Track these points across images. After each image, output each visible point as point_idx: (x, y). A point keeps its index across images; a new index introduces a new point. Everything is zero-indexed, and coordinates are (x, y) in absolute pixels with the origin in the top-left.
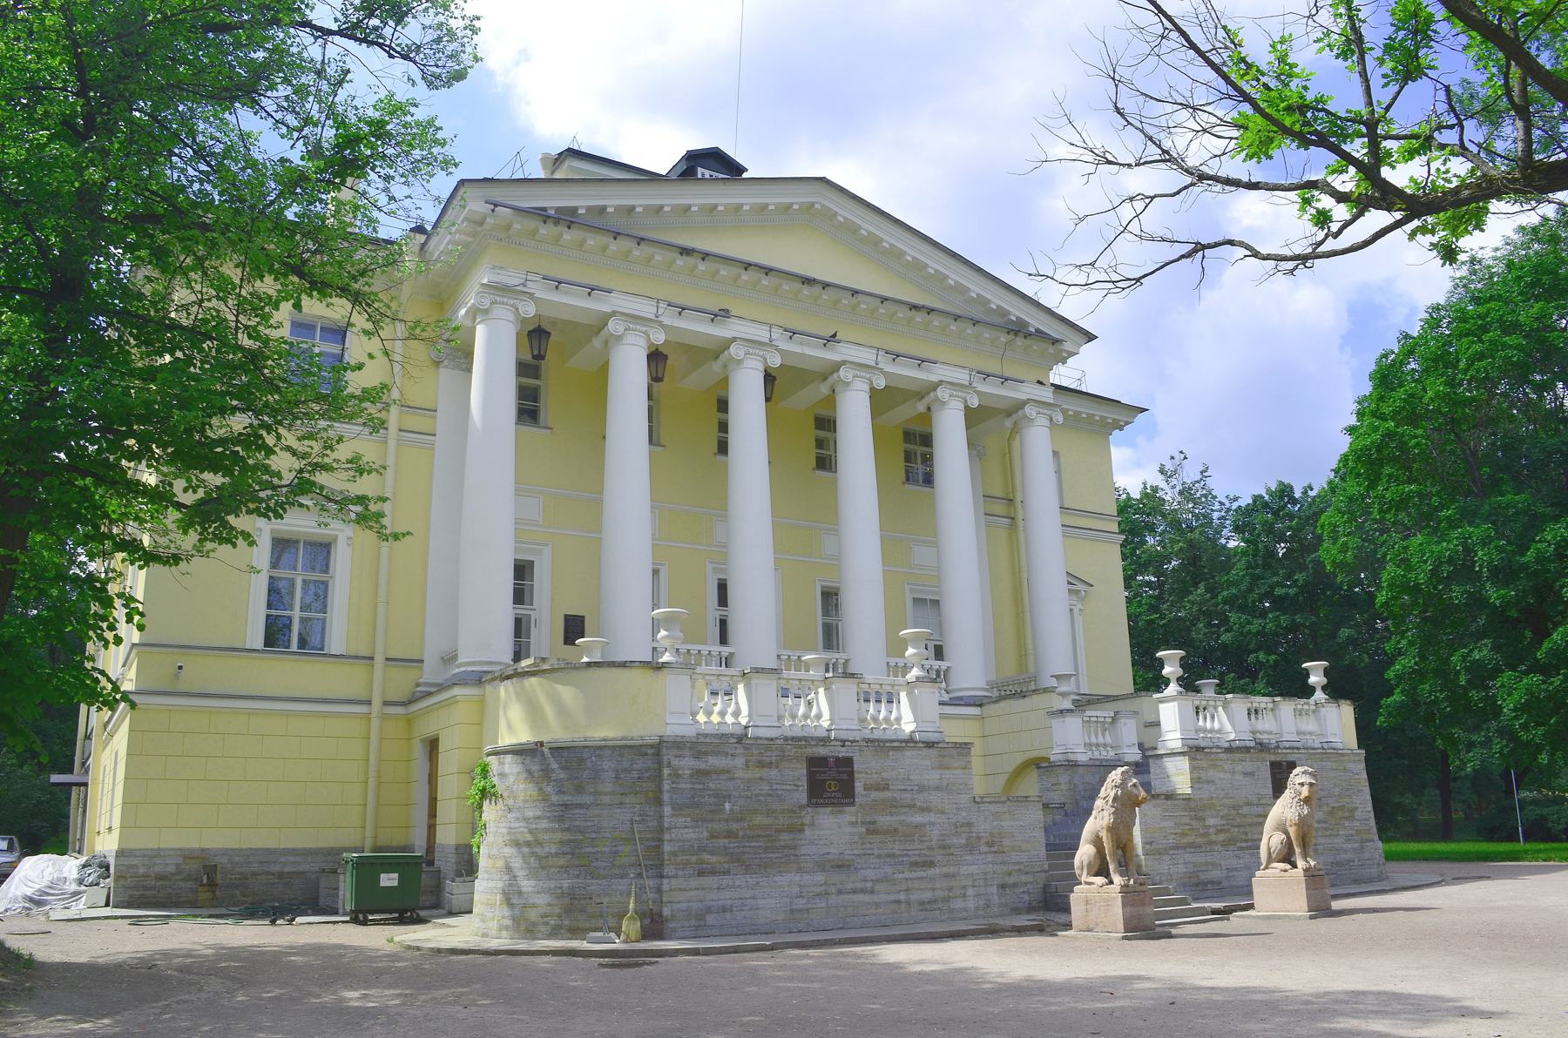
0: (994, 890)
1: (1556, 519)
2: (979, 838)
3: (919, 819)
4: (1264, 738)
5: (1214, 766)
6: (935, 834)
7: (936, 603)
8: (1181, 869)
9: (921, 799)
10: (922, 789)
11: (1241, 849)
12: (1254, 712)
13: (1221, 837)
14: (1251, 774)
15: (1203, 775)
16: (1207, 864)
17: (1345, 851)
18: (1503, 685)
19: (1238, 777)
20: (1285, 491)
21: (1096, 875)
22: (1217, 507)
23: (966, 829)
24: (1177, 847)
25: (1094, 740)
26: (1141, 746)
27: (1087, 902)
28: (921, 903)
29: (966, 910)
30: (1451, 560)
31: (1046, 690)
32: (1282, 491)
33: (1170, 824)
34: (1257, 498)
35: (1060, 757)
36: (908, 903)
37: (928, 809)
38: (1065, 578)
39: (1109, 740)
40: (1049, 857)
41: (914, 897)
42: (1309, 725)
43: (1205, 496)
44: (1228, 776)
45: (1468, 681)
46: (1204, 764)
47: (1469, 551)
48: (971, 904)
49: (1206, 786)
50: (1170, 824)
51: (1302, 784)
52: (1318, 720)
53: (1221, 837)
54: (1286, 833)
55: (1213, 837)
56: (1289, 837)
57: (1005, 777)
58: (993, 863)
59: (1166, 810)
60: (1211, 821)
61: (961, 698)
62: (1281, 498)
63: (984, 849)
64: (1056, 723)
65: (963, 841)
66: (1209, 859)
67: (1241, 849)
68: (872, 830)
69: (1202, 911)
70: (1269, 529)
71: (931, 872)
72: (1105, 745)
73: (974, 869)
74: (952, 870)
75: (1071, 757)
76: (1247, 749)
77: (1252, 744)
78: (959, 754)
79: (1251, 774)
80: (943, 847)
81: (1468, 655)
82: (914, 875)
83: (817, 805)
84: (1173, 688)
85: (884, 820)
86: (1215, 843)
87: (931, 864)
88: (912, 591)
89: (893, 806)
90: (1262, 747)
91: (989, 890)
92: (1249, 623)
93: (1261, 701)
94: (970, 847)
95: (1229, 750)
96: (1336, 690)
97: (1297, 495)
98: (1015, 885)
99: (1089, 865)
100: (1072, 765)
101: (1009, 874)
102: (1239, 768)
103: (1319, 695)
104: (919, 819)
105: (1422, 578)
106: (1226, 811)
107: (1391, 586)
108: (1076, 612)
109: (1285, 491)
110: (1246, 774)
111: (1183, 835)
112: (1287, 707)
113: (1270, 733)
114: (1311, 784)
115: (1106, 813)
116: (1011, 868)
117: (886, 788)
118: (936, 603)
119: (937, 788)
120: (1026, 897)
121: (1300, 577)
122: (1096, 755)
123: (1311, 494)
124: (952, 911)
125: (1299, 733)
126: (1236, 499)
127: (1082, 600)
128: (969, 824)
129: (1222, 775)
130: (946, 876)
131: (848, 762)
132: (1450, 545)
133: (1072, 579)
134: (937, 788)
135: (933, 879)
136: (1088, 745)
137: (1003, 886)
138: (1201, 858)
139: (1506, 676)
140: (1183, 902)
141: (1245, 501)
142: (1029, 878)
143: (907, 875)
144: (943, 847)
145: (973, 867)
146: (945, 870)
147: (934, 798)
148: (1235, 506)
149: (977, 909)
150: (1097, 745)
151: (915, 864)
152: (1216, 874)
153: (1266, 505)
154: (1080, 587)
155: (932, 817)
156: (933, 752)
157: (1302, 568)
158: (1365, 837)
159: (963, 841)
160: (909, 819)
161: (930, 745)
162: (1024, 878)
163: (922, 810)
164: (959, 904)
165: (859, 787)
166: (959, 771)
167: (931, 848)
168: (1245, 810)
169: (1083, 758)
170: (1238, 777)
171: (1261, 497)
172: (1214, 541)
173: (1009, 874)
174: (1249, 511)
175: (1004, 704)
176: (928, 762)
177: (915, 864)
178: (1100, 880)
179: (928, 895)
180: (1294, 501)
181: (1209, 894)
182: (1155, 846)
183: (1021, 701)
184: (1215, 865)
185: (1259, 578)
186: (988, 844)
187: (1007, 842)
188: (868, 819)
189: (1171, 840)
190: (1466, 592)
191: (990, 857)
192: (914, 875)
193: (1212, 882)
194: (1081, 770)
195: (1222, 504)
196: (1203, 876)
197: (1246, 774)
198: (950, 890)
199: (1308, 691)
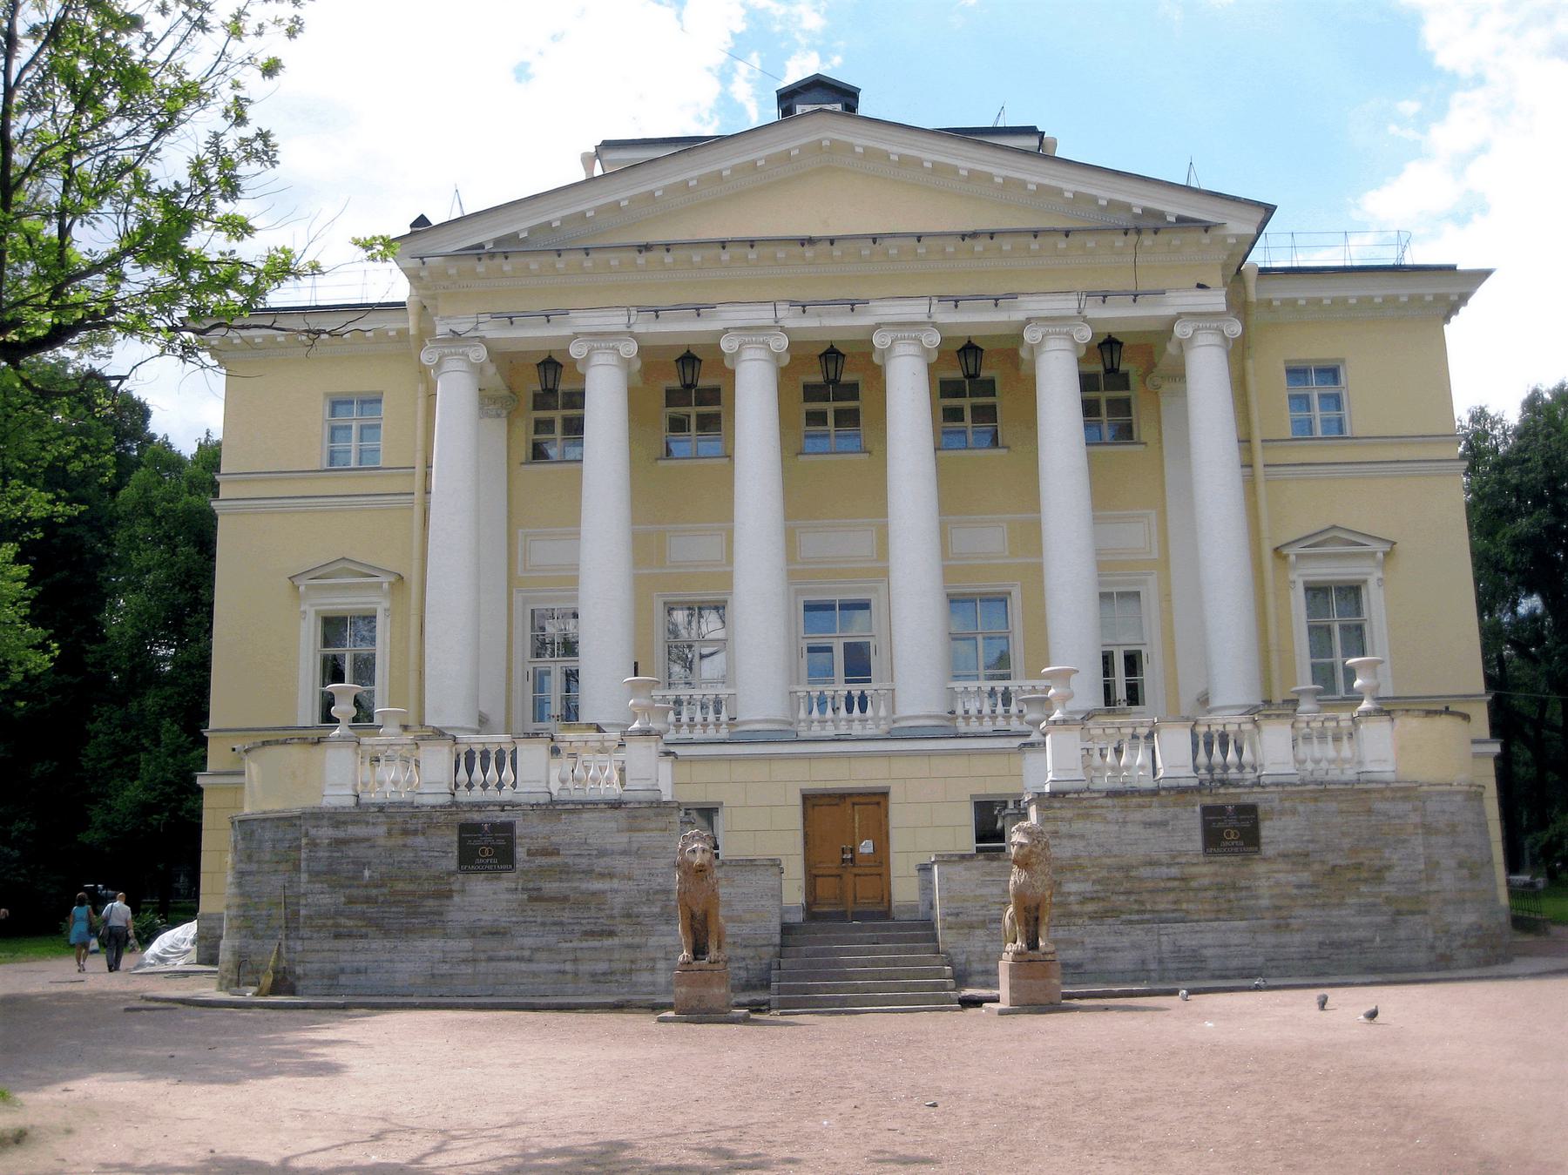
68: (536, 897)
83: (467, 872)
85: (551, 887)
89: (565, 872)
117: (556, 852)
131: (508, 827)
165: (520, 853)
188: (531, 885)
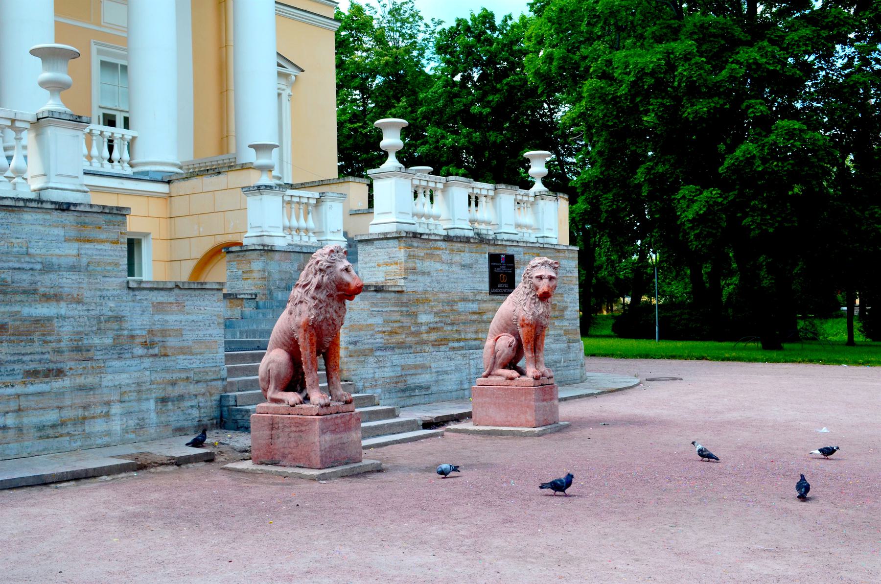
0: (152, 404)
1: (750, 44)
2: (132, 337)
3: (42, 310)
4: (483, 228)
5: (430, 256)
6: (66, 330)
7: (124, 68)
8: (388, 373)
9: (46, 282)
10: (48, 268)
11: (453, 349)
12: (474, 201)
13: (433, 336)
14: (469, 266)
15: (419, 265)
16: (416, 367)
17: (553, 351)
18: (684, 197)
19: (455, 269)
20: (487, 18)
21: (287, 388)
22: (422, 28)
23: (115, 326)
24: (384, 348)
25: (294, 223)
26: (345, 234)
27: (273, 426)
28: (41, 428)
29: (108, 433)
30: (653, 74)
31: (245, 167)
32: (485, 17)
33: (379, 320)
34: (460, 22)
35: (254, 241)
36: (20, 429)
37: (57, 298)
38: (274, 59)
39: (311, 224)
40: (229, 359)
41: (31, 419)
42: (526, 217)
43: (413, 16)
44: (446, 267)
45: (650, 192)
46: (421, 253)
47: (671, 67)
48: (116, 426)
49: (420, 278)
50: (379, 320)
51: (540, 278)
52: (535, 213)
53: (433, 336)
54: (516, 334)
55: (425, 336)
56: (519, 341)
57: (195, 262)
58: (152, 370)
59: (374, 305)
60: (423, 318)
61: (147, 173)
62: (484, 23)
63: (139, 351)
64: (253, 202)
65: (108, 341)
66: (419, 360)
67: (453, 349)
69: (410, 425)
70: (469, 50)
71: (57, 384)
72: (307, 230)
73: (123, 378)
74: (90, 380)
75: (267, 241)
76: (467, 240)
77: (471, 234)
78: (108, 223)
79: (469, 266)
80: (78, 349)
81: (653, 168)
82: (31, 389)
84: (392, 162)
86: (425, 343)
87: (60, 373)
88: (99, 52)
90: (481, 239)
91: (144, 406)
92: (443, 137)
93: (484, 188)
94: (120, 348)
95: (448, 239)
96: (556, 183)
97: (498, 22)
98: (181, 398)
99: (278, 376)
100: (268, 251)
101: (173, 384)
102: (457, 258)
103: (539, 187)
104: (42, 310)
105: (623, 90)
106: (440, 307)
107: (592, 97)
108: (284, 97)
109: (487, 18)
110: (463, 266)
111: (392, 333)
112: (507, 196)
113: (488, 223)
114: (551, 278)
115: (304, 307)
116: (176, 376)
118: (124, 68)
119: (73, 268)
120: (195, 413)
121: (494, 98)
122: (296, 240)
123: (509, 23)
124: (88, 436)
125: (518, 226)
126: (440, 23)
127: (293, 85)
128: (119, 319)
129: (438, 266)
130: (81, 388)
132: (650, 58)
133: (283, 60)
134: (73, 268)
135: (60, 394)
136: (289, 229)
137: (164, 400)
138: (411, 360)
139: (686, 191)
140: (391, 413)
141: (449, 23)
142: (201, 388)
143: (19, 389)
144: (78, 349)
145: (121, 374)
146: (80, 381)
147: (67, 282)
148: (439, 28)
149: (126, 431)
150: (298, 230)
151: (34, 374)
152: (424, 378)
153: (468, 29)
154: (290, 70)
155: (63, 309)
156: (68, 218)
157: (495, 91)
158: (572, 337)
159: (108, 341)
160: (26, 311)
161: (64, 207)
162: (192, 389)
163: (47, 298)
164: (99, 426)
166: (107, 246)
167: (59, 351)
168: (460, 306)
169: (280, 243)
170: (455, 269)
171: (466, 21)
172: (417, 63)
173: (173, 384)
174: (453, 34)
175: (195, 182)
176: (60, 232)
177: (34, 374)
178: (292, 397)
179: (52, 416)
180: (493, 28)
181: (416, 400)
182: (360, 346)
183: (215, 179)
184: (424, 367)
185: (456, 95)
186: (145, 344)
187: (172, 342)
189: (379, 339)
190: (662, 104)
191: (147, 362)
192: (31, 389)
193: (420, 388)
194: (277, 256)
195: (427, 26)
196: (411, 381)
197: (463, 266)
198: (85, 408)
199: (527, 184)
